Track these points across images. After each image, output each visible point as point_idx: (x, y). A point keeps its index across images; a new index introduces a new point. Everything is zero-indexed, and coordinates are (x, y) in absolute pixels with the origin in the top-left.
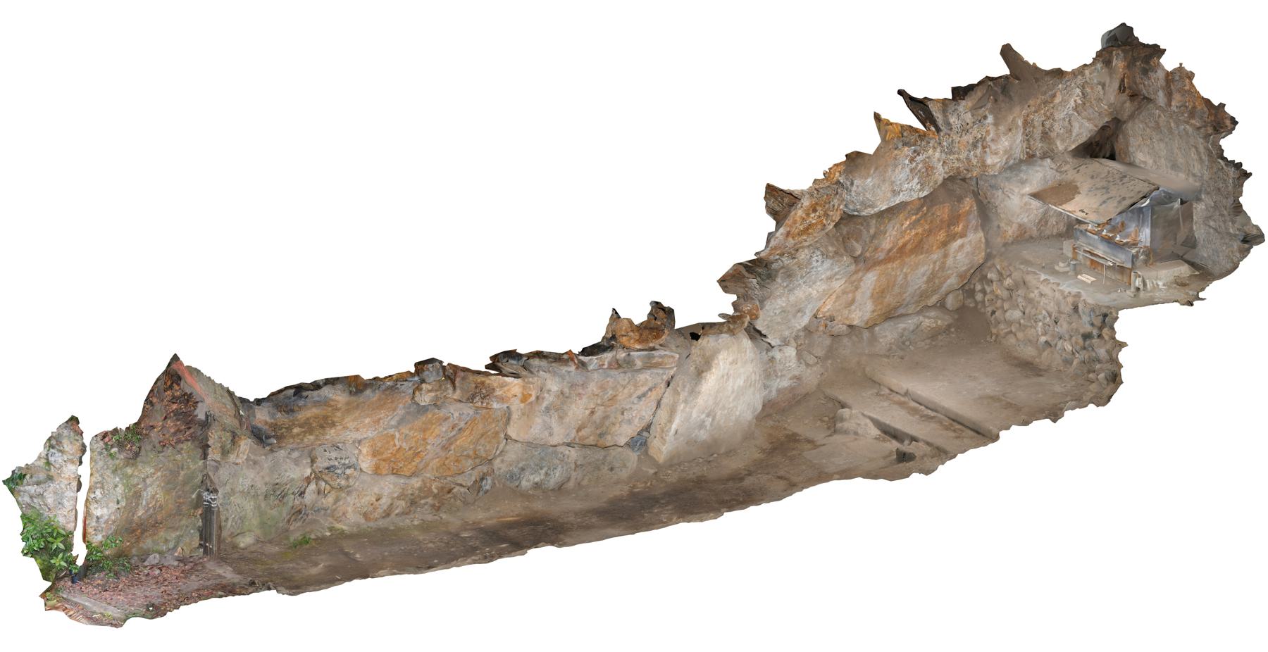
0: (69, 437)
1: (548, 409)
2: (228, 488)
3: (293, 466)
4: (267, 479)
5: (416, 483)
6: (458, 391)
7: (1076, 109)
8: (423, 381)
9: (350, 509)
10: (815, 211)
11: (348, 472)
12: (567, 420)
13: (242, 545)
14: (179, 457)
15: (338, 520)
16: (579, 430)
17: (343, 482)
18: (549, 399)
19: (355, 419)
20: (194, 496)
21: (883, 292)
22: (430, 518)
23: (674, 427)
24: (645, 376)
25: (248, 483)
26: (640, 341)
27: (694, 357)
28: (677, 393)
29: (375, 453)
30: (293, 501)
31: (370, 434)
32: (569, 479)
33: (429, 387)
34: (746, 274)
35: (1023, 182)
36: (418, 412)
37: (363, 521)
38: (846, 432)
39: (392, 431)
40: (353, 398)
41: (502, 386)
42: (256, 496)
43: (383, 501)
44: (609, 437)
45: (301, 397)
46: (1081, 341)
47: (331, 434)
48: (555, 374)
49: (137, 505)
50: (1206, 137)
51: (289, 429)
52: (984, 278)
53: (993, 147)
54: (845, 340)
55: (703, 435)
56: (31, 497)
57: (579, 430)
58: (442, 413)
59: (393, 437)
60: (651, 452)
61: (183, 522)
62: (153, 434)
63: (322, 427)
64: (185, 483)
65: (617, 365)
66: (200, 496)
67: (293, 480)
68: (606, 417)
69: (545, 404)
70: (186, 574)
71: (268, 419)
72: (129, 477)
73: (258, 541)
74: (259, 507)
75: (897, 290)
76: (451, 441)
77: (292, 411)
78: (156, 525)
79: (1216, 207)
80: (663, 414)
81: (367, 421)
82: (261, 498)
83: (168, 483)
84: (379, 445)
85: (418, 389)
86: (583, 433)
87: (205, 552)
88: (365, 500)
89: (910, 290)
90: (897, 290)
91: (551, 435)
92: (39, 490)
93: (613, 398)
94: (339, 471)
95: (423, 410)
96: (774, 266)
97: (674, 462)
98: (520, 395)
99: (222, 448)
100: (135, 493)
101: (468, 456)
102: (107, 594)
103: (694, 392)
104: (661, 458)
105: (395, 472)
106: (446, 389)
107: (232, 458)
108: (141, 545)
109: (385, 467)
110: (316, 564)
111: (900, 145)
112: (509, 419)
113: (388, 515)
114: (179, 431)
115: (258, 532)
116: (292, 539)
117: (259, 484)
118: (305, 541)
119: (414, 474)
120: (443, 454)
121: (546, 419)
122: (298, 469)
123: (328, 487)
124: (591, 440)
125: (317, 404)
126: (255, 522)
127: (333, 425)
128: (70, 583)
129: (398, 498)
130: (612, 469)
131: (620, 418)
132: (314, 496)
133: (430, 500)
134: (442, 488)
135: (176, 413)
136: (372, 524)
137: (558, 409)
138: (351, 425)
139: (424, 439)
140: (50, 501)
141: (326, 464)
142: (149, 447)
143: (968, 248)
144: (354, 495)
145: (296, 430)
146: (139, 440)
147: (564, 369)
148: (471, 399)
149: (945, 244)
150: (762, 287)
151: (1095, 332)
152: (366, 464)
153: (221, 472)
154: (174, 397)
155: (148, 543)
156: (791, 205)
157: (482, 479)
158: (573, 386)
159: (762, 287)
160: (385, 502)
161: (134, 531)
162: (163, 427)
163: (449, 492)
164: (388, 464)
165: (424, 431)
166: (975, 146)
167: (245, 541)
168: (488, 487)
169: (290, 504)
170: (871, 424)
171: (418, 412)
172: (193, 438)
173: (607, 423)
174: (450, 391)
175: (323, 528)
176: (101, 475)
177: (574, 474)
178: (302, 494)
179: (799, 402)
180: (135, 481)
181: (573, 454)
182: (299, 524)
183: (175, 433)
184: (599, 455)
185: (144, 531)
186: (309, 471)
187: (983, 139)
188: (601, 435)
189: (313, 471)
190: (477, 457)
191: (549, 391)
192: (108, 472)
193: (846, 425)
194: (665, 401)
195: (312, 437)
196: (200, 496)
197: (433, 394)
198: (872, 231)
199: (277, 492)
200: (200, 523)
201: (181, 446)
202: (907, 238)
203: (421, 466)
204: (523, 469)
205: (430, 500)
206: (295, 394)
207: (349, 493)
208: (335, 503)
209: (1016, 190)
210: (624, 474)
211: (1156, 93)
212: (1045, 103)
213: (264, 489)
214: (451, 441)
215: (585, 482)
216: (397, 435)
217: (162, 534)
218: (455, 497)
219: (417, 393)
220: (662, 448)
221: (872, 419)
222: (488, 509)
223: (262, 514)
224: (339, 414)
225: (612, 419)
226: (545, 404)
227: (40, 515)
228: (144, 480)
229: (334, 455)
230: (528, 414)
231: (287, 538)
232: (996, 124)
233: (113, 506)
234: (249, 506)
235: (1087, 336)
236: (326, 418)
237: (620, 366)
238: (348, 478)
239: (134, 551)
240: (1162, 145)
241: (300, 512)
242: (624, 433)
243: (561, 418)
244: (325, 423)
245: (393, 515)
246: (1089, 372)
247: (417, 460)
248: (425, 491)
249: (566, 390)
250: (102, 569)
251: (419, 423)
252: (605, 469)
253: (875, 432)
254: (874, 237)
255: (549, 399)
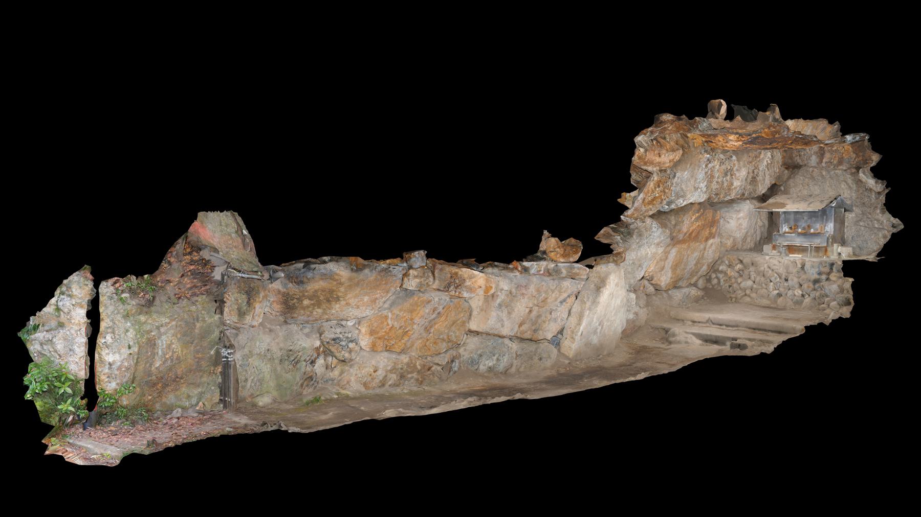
0: (79, 282)
1: (500, 305)
2: (246, 350)
3: (304, 337)
4: (282, 345)
5: (405, 359)
6: (437, 282)
7: (767, 166)
8: (410, 267)
9: (353, 379)
10: (659, 186)
11: (351, 345)
12: (513, 315)
13: (261, 404)
14: (193, 308)
15: (343, 388)
16: (520, 325)
17: (347, 355)
18: (502, 297)
19: (356, 297)
20: (212, 352)
21: (676, 265)
22: (415, 389)
23: (582, 328)
24: (567, 283)
25: (264, 347)
26: (564, 256)
27: (592, 279)
28: (583, 302)
29: (372, 333)
30: (304, 367)
31: (368, 312)
32: (512, 365)
33: (416, 273)
34: (613, 233)
35: (739, 211)
36: (407, 296)
37: (363, 389)
38: (679, 342)
39: (385, 313)
40: (354, 274)
41: (471, 278)
42: (272, 359)
43: (379, 372)
44: (541, 332)
45: (310, 269)
46: (811, 285)
47: (336, 308)
48: (505, 277)
49: (154, 354)
50: (852, 174)
51: (300, 300)
52: (716, 271)
53: (738, 175)
54: (654, 297)
55: (595, 340)
56: (41, 344)
57: (520, 325)
58: (426, 297)
59: (386, 317)
60: (563, 350)
61: (204, 379)
62: (169, 288)
63: (328, 301)
64: (202, 337)
65: (548, 273)
66: (218, 353)
67: (304, 348)
68: (539, 316)
69: (498, 301)
70: (202, 422)
71: (281, 288)
72: (142, 324)
73: (275, 401)
74: (275, 370)
75: (683, 266)
76: (432, 323)
77: (302, 282)
78: (177, 379)
79: (863, 214)
80: (573, 320)
81: (366, 299)
82: (277, 361)
83: (185, 335)
84: (375, 325)
85: (406, 275)
86: (524, 328)
87: (225, 407)
88: (364, 371)
89: (688, 268)
90: (683, 266)
91: (503, 326)
92: (49, 336)
93: (545, 301)
94: (343, 343)
95: (409, 293)
96: (632, 227)
97: (578, 356)
98: (483, 287)
99: (239, 310)
100: (149, 340)
101: (443, 340)
102: (114, 438)
103: (595, 302)
104: (571, 354)
105: (388, 349)
106: (429, 276)
107: (248, 319)
108: (164, 400)
109: (380, 344)
110: (326, 413)
111: (703, 151)
112: (470, 315)
113: (383, 385)
114: (195, 286)
115: (275, 393)
116: (305, 401)
117: (275, 349)
118: (317, 400)
119: (403, 352)
120: (425, 335)
121: (500, 313)
122: (309, 341)
123: (335, 361)
124: (527, 335)
125: (324, 277)
126: (272, 384)
127: (338, 299)
128: (81, 430)
129: (391, 371)
130: (541, 359)
131: (549, 317)
132: (323, 369)
133: (415, 375)
134: (424, 366)
135: (194, 273)
136: (370, 391)
137: (506, 305)
138: (353, 302)
139: (412, 319)
140: (60, 346)
141: (333, 336)
142: (164, 298)
143: (714, 247)
144: (356, 367)
145: (306, 302)
146: (154, 290)
147: (511, 275)
148: (447, 288)
149: (707, 239)
150: (624, 241)
151: (824, 277)
152: (365, 342)
153: (240, 337)
154: (192, 260)
155: (170, 399)
156: (648, 177)
157: (452, 361)
158: (518, 287)
159: (624, 241)
160: (381, 373)
161: (155, 385)
162: (179, 282)
163: (429, 370)
164: (384, 342)
165: (411, 311)
166: (726, 175)
167: (264, 401)
168: (456, 369)
169: (303, 370)
170: (694, 338)
171: (407, 296)
172: (208, 292)
173: (540, 321)
174: (431, 279)
175: (332, 392)
176: (112, 320)
177: (515, 361)
178: (313, 362)
179: (636, 331)
180: (148, 327)
181: (515, 346)
182: (311, 390)
183: (191, 288)
184: (532, 347)
185: (165, 386)
186: (318, 343)
187: (731, 170)
188: (535, 331)
189: (322, 342)
190: (450, 341)
191: (502, 290)
192: (119, 317)
193: (678, 338)
194: (573, 310)
195: (320, 311)
196: (218, 353)
197: (417, 280)
198: (673, 222)
199: (291, 358)
200: (220, 380)
201: (196, 298)
202: (694, 227)
203: (409, 344)
204: (481, 356)
205: (415, 375)
206: (304, 267)
207: (351, 366)
208: (340, 375)
209: (734, 216)
210: (548, 363)
211: (809, 158)
212: (756, 157)
213: (279, 354)
214: (432, 323)
215: (522, 369)
216: (390, 315)
217: (184, 389)
218: (433, 374)
219: (406, 279)
220: (571, 347)
221: (694, 334)
222: (459, 383)
223: (278, 377)
224: (342, 289)
225: (543, 318)
226: (498, 301)
227: (50, 362)
228: (158, 328)
229: (338, 330)
230: (484, 310)
231: (301, 400)
232: (738, 160)
233: (125, 352)
234: (266, 368)
235: (816, 281)
236: (331, 291)
237: (550, 275)
238: (350, 352)
239: (158, 406)
240: (816, 187)
241: (311, 378)
242: (550, 330)
243: (509, 313)
244: (331, 297)
245: (387, 386)
246: (819, 304)
247: (406, 338)
248: (411, 366)
249: (514, 290)
250: (117, 417)
251: (407, 305)
252: (536, 359)
253: (698, 342)
254: (675, 225)
255: (502, 297)
